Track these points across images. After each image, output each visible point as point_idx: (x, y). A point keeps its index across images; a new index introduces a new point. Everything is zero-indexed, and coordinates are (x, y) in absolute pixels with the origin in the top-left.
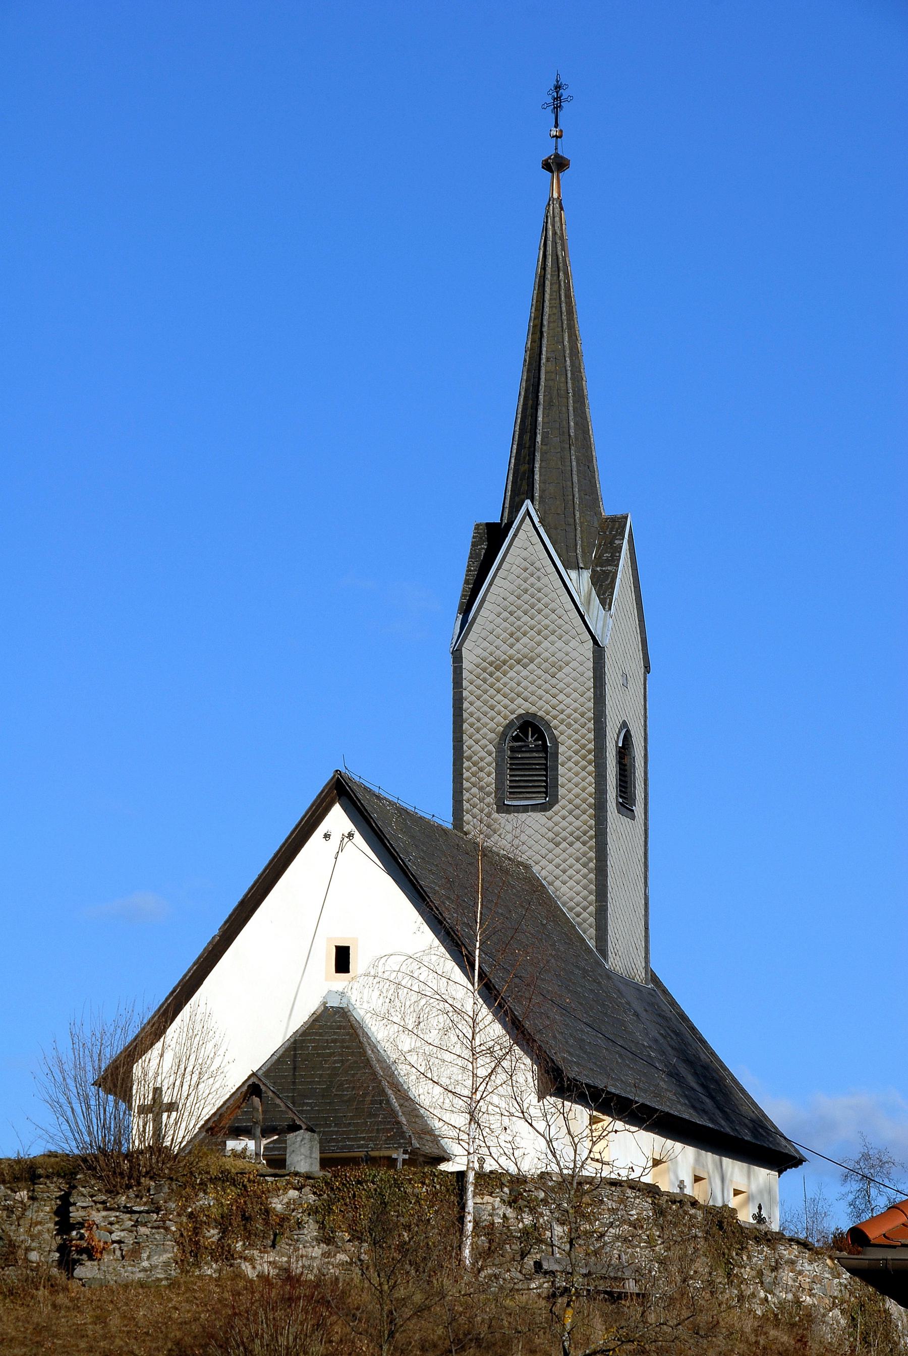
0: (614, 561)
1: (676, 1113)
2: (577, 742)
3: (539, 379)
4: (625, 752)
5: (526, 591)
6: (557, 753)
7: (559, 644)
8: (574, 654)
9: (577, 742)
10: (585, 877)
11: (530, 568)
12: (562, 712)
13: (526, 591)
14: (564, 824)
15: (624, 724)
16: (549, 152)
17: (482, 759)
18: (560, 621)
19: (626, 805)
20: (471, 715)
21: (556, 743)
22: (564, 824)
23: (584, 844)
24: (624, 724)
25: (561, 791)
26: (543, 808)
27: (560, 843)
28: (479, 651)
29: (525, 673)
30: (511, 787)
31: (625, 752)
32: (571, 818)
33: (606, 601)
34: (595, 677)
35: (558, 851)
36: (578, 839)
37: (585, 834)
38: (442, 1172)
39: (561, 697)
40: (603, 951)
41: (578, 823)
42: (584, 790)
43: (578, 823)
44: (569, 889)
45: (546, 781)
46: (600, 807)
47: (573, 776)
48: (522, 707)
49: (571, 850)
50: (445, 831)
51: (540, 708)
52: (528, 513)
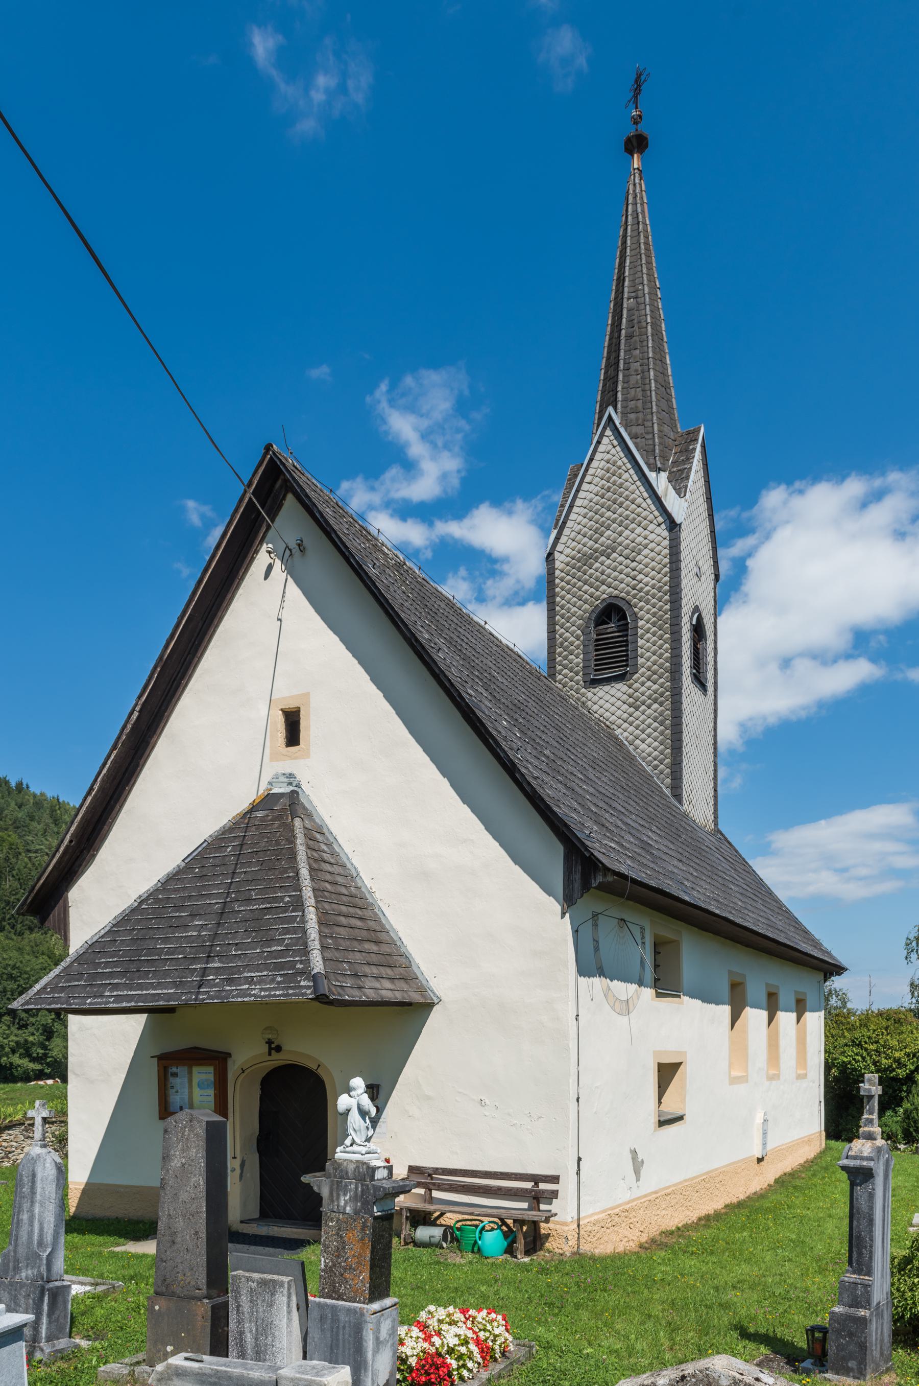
0: (689, 459)
1: (204, 1204)
2: (654, 615)
3: (622, 315)
4: (698, 630)
5: (608, 490)
6: (637, 627)
7: (639, 530)
8: (652, 537)
9: (654, 615)
10: (662, 733)
11: (611, 471)
12: (640, 590)
13: (608, 490)
14: (643, 689)
15: (696, 609)
16: (631, 131)
17: (572, 644)
18: (640, 510)
19: (699, 680)
20: (562, 607)
21: (636, 618)
22: (643, 689)
23: (661, 704)
24: (696, 609)
25: (641, 661)
26: (621, 678)
27: (639, 707)
28: (568, 551)
29: (608, 562)
30: (596, 665)
31: (698, 630)
32: (649, 683)
33: (681, 491)
34: (671, 547)
35: (637, 714)
36: (655, 701)
37: (660, 647)
38: (94, 949)
39: (640, 577)
40: (678, 797)
41: (655, 687)
42: (660, 656)
43: (655, 687)
44: (647, 747)
45: (627, 641)
46: (675, 672)
47: (649, 646)
48: (605, 592)
49: (649, 711)
50: (533, 673)
51: (621, 588)
52: (610, 417)
